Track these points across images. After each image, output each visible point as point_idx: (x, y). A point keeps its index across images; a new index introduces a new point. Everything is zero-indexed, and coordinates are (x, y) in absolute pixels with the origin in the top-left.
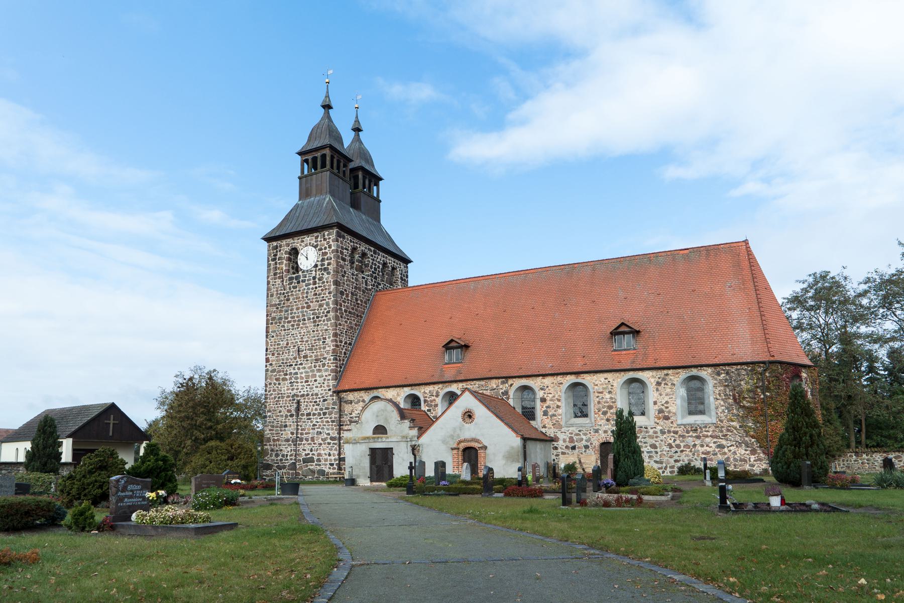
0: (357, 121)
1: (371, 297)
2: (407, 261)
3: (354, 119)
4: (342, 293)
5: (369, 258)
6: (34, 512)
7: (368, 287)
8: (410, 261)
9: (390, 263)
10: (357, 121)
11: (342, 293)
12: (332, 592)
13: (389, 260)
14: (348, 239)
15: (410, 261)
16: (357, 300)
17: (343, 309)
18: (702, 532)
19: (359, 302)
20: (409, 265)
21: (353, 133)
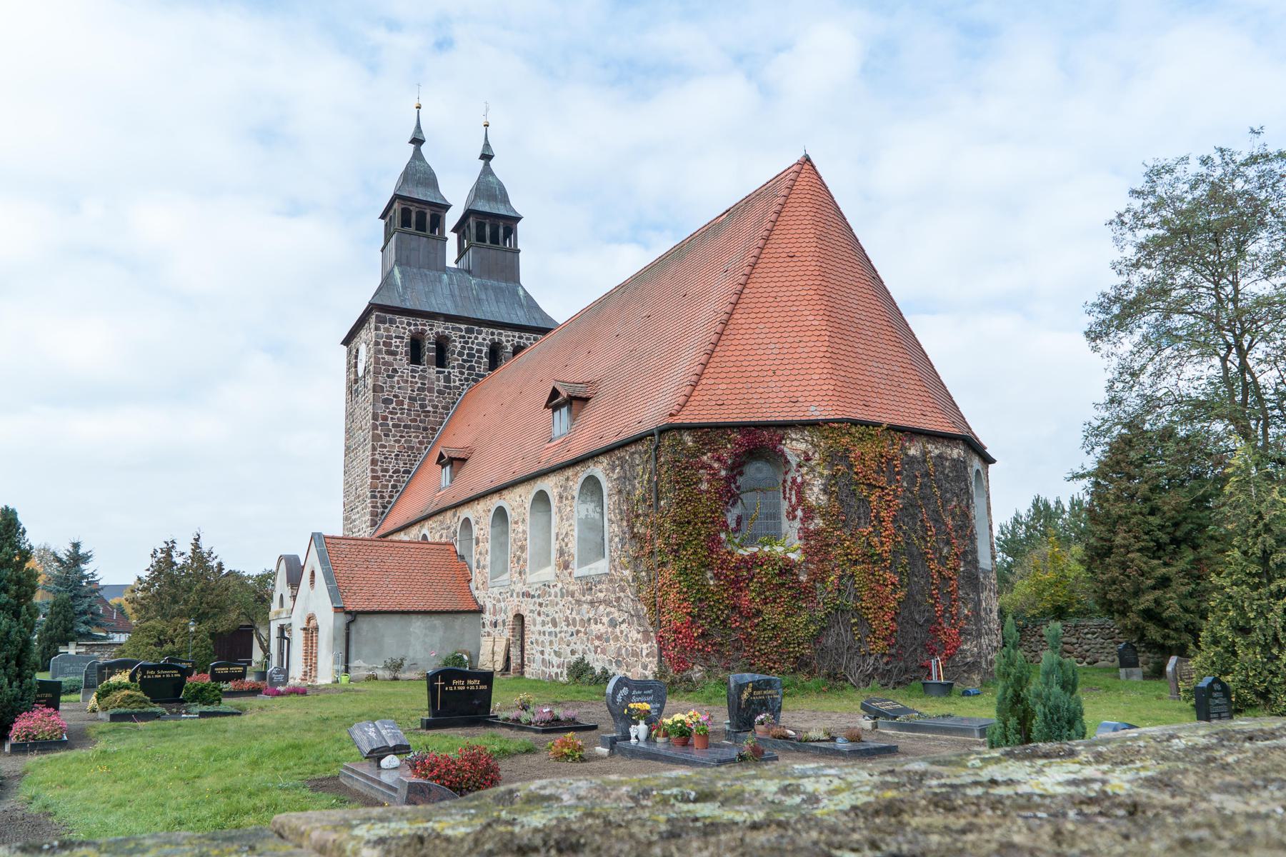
0: (487, 145)
1: (460, 398)
2: (988, 460)
3: (483, 142)
4: (387, 402)
5: (455, 341)
6: (1213, 765)
7: (452, 385)
8: (993, 461)
9: (508, 341)
10: (487, 145)
11: (387, 402)
12: (67, 657)
13: (528, 339)
14: (401, 323)
15: (993, 461)
16: (423, 406)
17: (391, 423)
18: (1045, 790)
19: (429, 408)
20: (991, 466)
21: (412, 146)
